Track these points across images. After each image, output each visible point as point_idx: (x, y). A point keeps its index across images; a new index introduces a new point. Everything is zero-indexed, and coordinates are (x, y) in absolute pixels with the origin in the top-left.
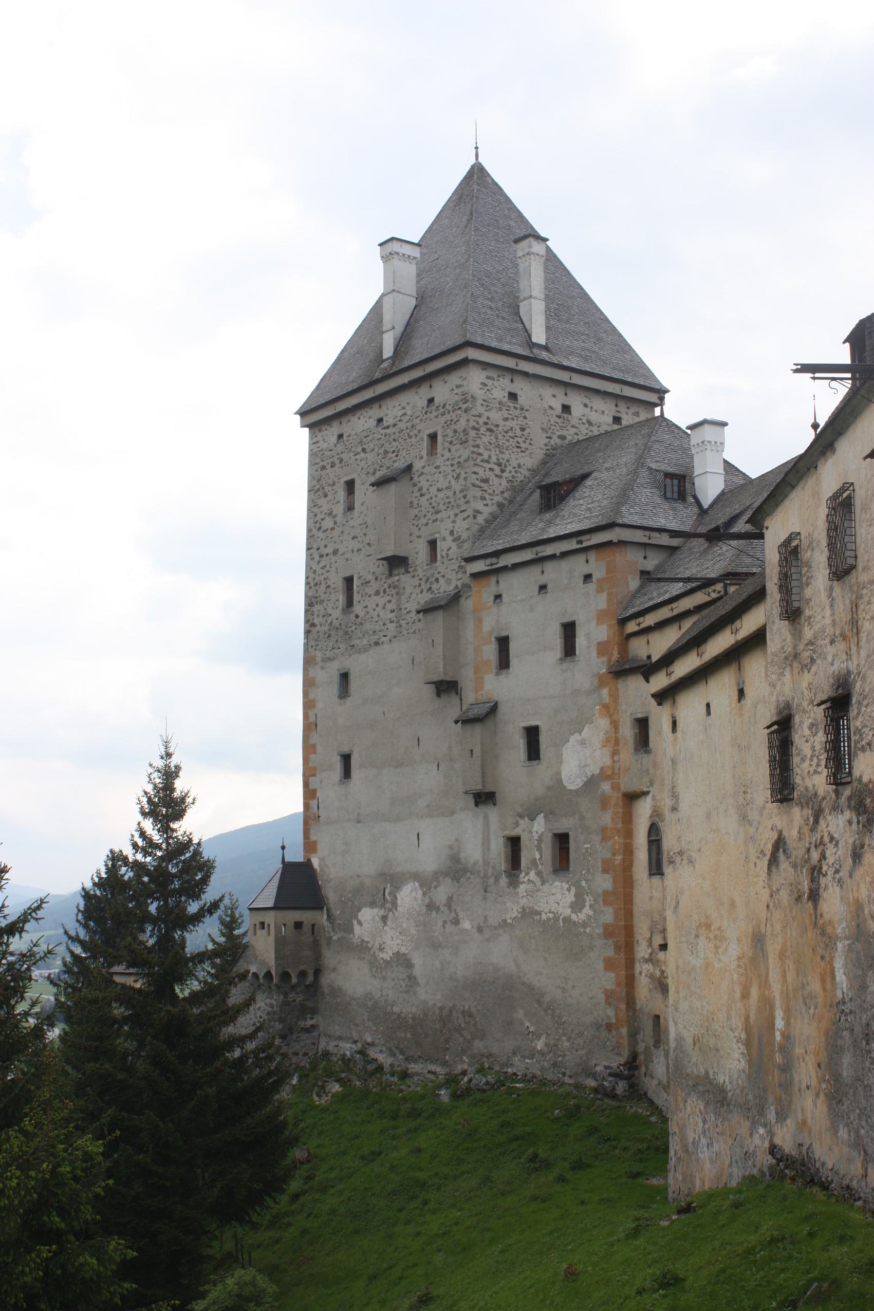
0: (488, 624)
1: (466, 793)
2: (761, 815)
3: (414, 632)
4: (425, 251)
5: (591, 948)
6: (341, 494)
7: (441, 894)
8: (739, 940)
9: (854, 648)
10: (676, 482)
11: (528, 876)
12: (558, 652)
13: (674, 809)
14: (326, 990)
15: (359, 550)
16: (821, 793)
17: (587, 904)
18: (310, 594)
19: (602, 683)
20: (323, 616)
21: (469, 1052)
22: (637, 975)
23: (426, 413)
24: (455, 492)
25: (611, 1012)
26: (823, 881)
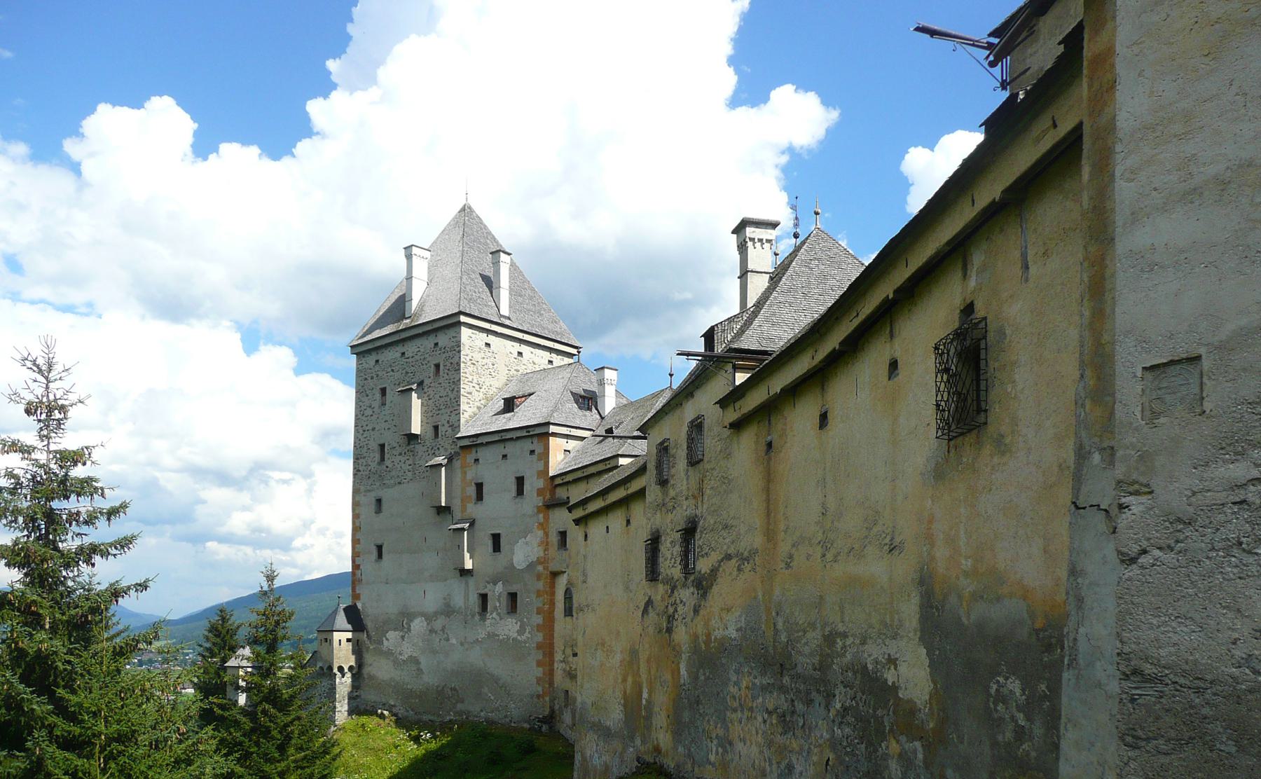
0: (469, 476)
1: (455, 569)
2: (638, 587)
3: (424, 478)
4: (433, 254)
5: (529, 654)
6: (378, 396)
7: (438, 624)
8: (621, 652)
11: (492, 616)
12: (514, 493)
14: (366, 676)
15: (389, 429)
16: (676, 577)
17: (527, 631)
18: (357, 453)
19: (539, 510)
20: (365, 466)
21: (454, 710)
22: (555, 669)
25: (540, 689)
26: (675, 623)
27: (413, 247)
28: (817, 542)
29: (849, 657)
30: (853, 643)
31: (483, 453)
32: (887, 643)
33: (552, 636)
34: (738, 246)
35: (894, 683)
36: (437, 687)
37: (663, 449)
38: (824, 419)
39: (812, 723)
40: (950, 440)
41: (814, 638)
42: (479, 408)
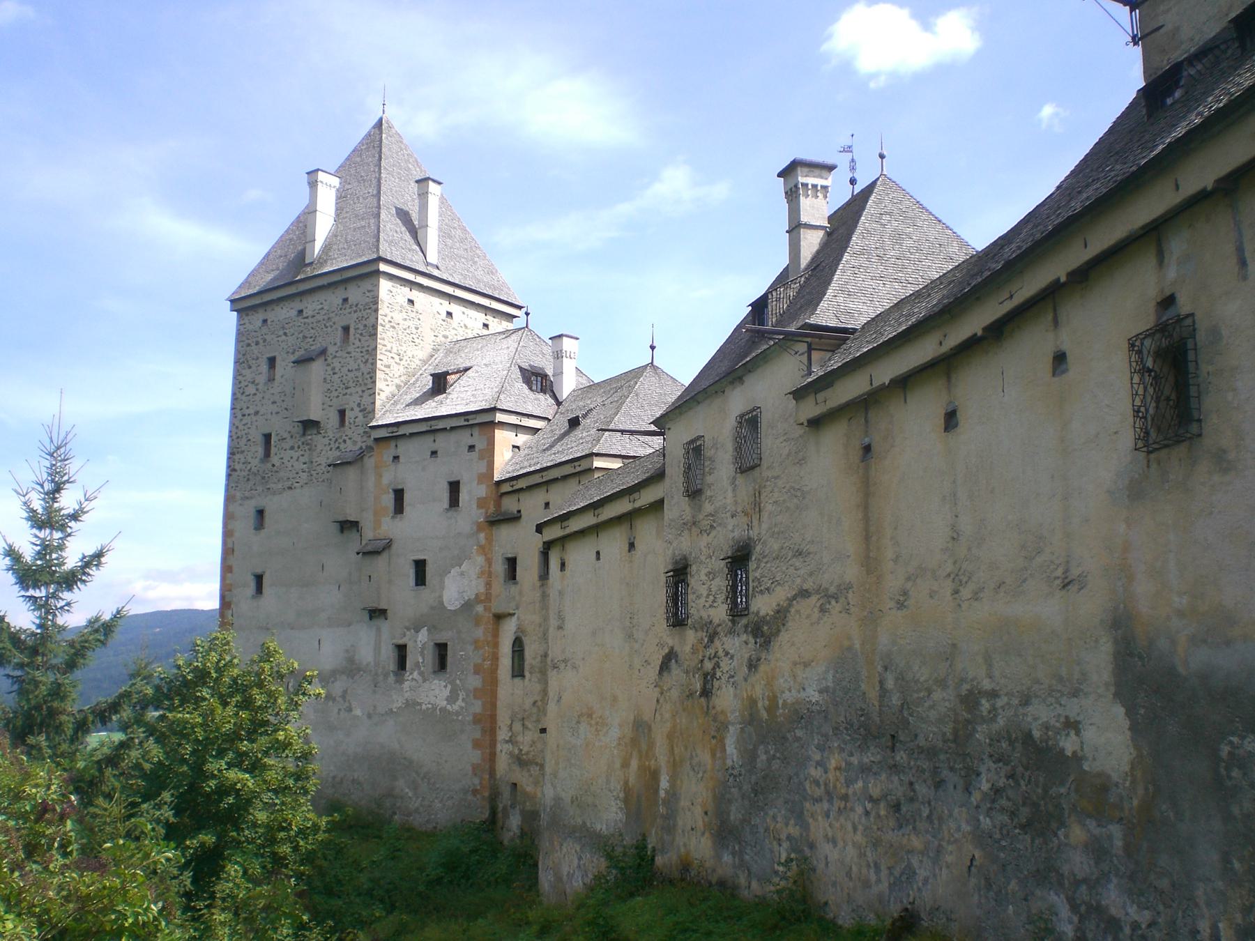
0: (385, 480)
3: (323, 481)
6: (264, 368)
7: (338, 687)
9: (755, 523)
10: (539, 379)
11: (412, 675)
12: (446, 504)
13: (560, 628)
15: (277, 413)
16: (716, 621)
17: (461, 697)
19: (480, 528)
20: (244, 463)
22: (498, 753)
23: (341, 309)
24: (363, 374)
25: (476, 781)
26: (716, 683)
27: (320, 172)
28: (945, 574)
29: (1001, 722)
30: (1008, 704)
31: (404, 448)
32: (1063, 702)
33: (494, 705)
34: (786, 193)
35: (1074, 753)
36: (334, 777)
37: (695, 450)
38: (951, 420)
39: (943, 812)
40: (1149, 452)
41: (943, 700)
42: (398, 387)
